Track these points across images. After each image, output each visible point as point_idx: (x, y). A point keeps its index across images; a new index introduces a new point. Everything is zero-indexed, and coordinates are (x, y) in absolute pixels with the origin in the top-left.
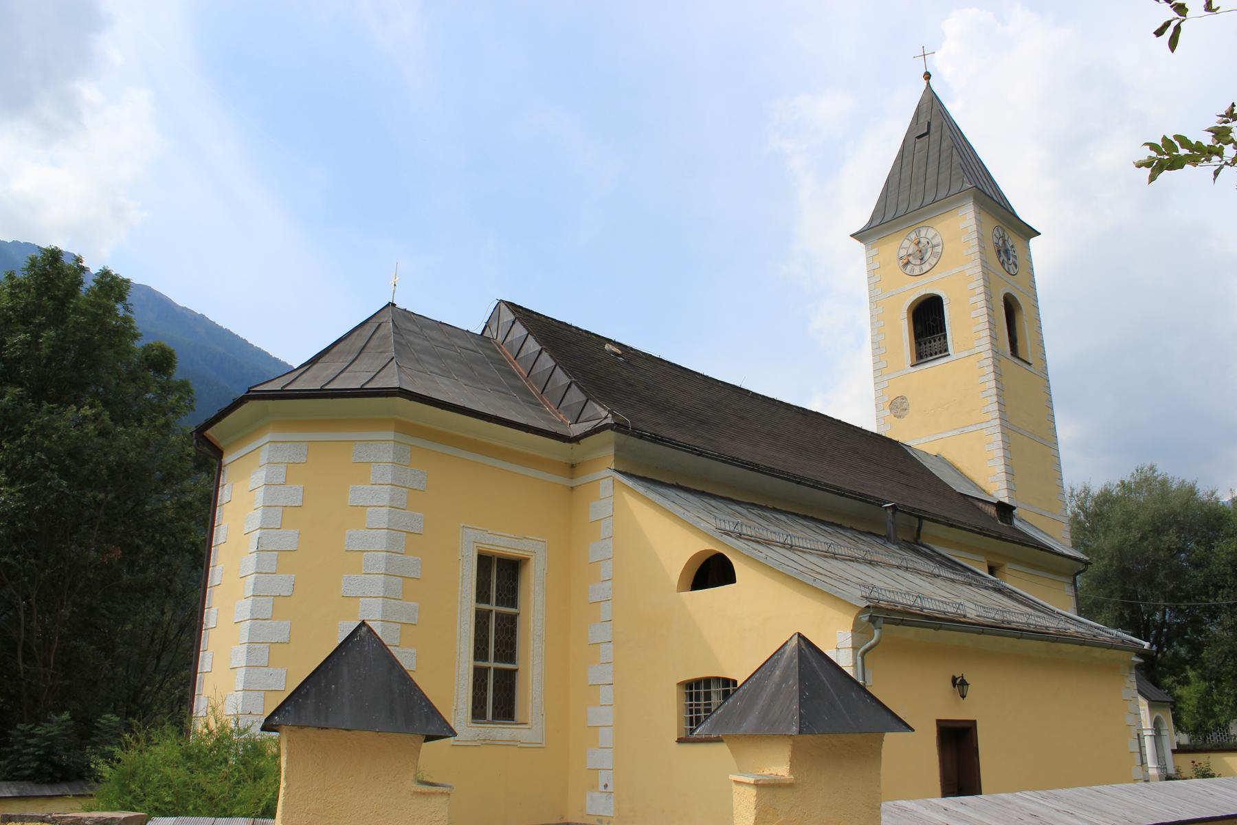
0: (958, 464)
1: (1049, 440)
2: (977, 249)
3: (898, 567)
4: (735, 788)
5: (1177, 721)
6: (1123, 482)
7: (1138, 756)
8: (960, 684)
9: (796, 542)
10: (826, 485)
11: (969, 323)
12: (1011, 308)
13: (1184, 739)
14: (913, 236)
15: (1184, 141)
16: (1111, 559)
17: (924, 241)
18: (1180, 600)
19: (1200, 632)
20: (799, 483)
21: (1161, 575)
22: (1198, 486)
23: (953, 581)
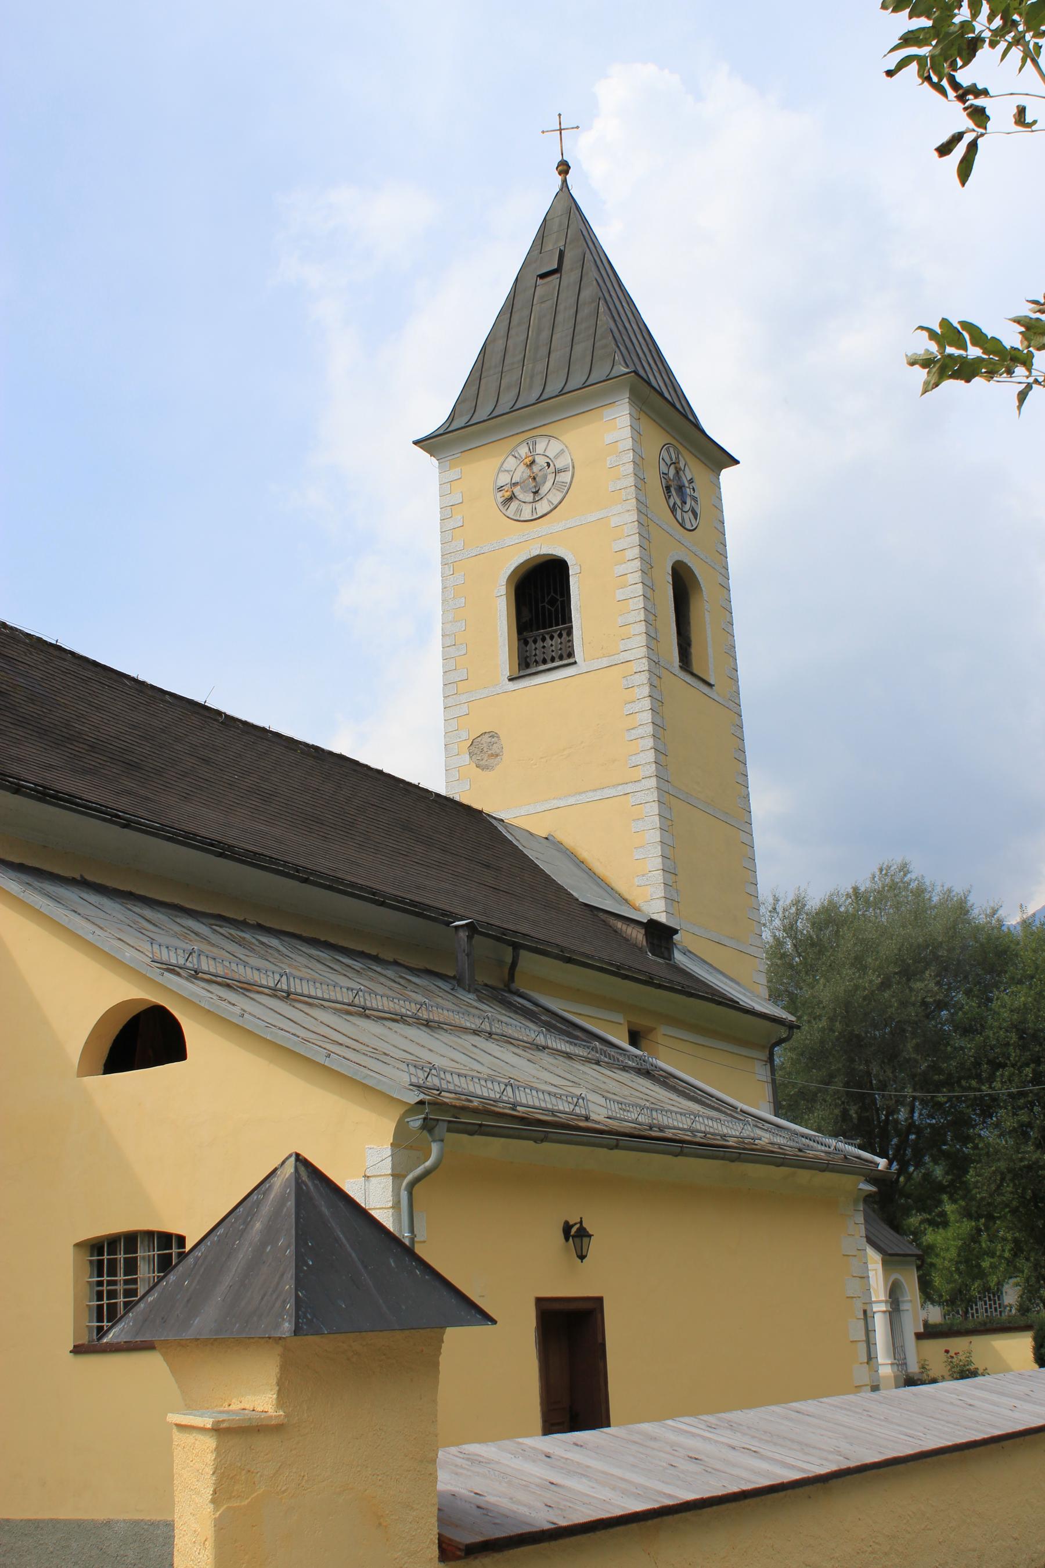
0: (584, 854)
1: (737, 816)
2: (631, 481)
3: (476, 1032)
4: (177, 1436)
5: (925, 1285)
6: (856, 889)
7: (863, 1347)
8: (576, 1236)
9: (297, 986)
10: (353, 885)
11: (611, 607)
12: (683, 586)
13: (935, 1314)
14: (523, 451)
15: (978, 337)
16: (832, 1020)
17: (541, 461)
18: (938, 1087)
19: (966, 1139)
20: (305, 881)
21: (910, 1045)
22: (972, 899)
23: (569, 1056)
